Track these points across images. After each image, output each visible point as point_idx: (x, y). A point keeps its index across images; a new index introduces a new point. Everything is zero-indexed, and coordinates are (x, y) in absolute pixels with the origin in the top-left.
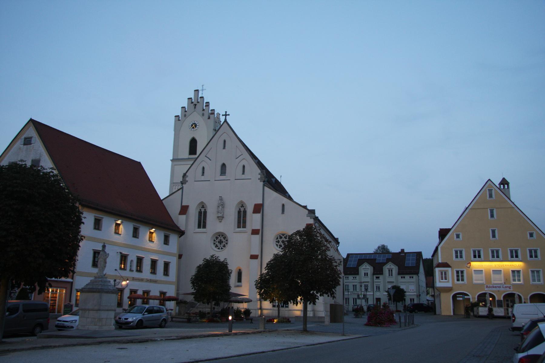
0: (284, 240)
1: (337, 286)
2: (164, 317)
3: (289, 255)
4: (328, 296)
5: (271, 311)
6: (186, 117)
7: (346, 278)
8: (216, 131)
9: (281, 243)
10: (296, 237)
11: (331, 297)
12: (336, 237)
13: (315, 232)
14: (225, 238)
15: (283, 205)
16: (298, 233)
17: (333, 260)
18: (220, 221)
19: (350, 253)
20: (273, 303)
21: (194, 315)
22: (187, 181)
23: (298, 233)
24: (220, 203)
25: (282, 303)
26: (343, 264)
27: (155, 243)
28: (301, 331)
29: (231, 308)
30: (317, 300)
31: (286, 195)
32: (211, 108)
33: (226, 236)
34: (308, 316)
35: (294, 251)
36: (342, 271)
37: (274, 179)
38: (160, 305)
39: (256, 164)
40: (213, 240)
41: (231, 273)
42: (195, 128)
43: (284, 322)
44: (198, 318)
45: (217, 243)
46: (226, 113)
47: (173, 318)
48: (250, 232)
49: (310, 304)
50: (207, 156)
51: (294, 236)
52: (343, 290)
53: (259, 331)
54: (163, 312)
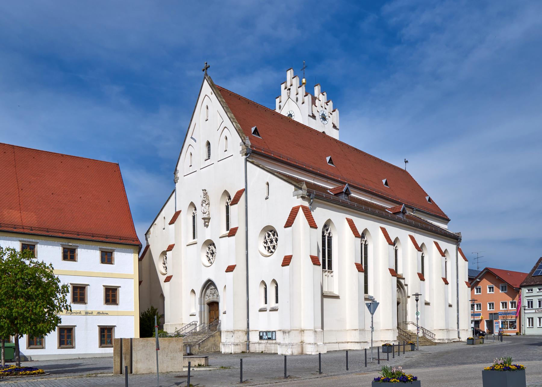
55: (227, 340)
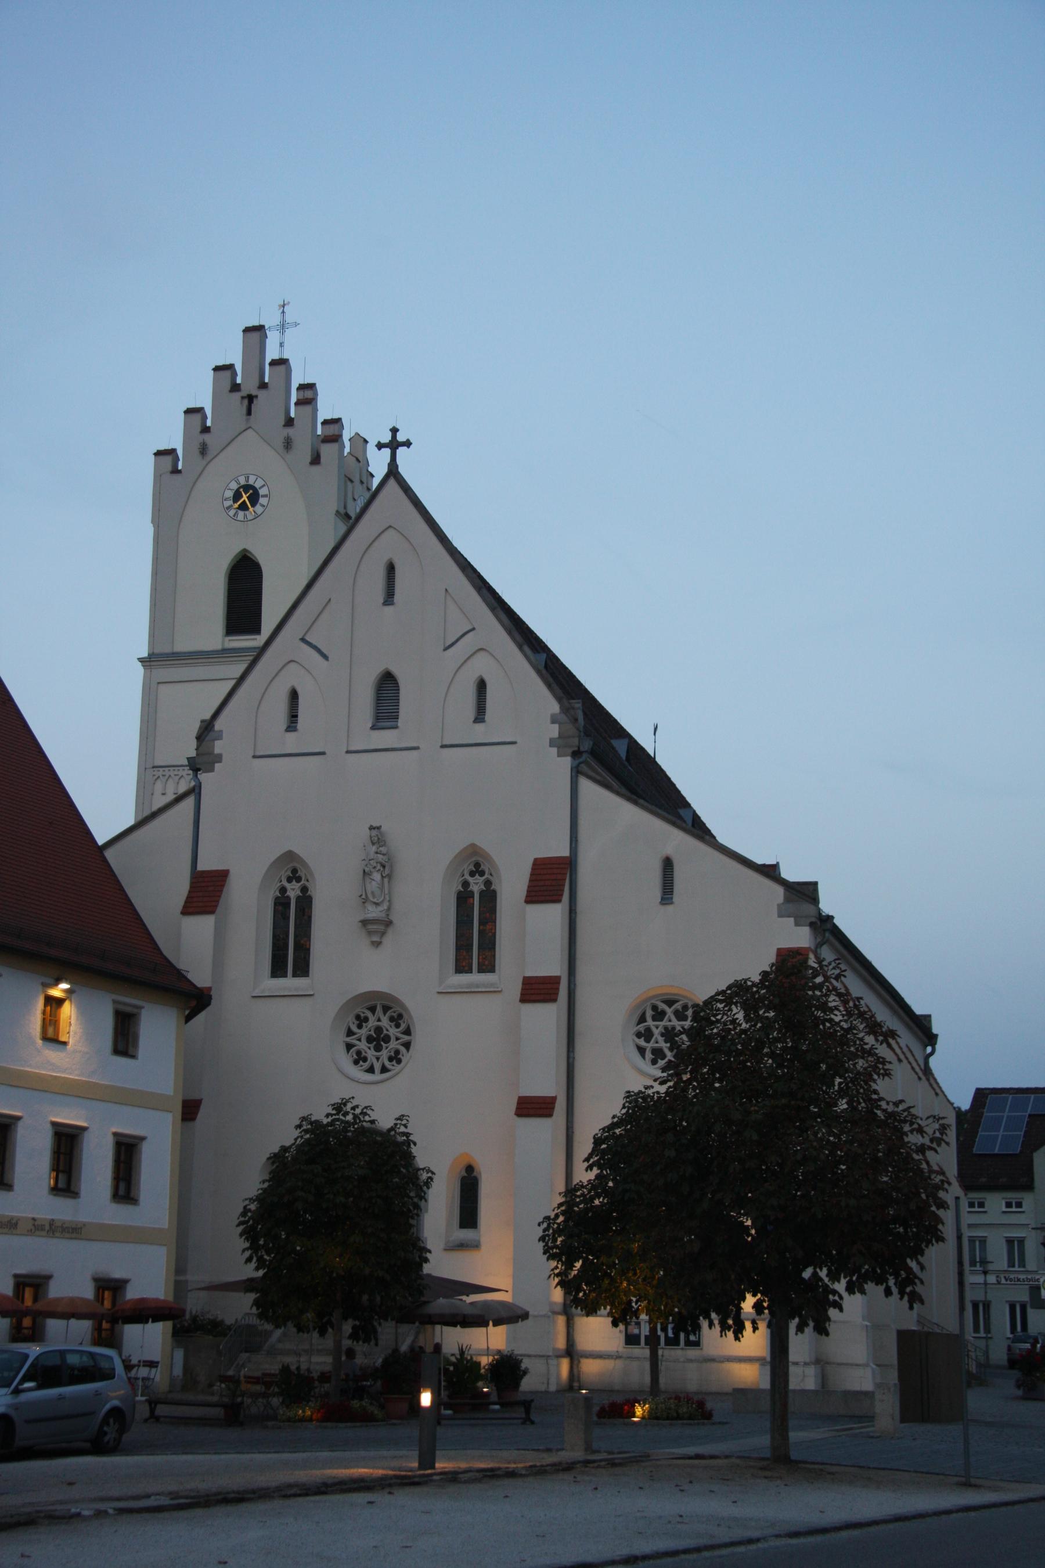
0: (674, 1028)
1: (929, 1243)
2: (116, 1403)
3: (694, 1097)
4: (888, 1292)
5: (619, 1363)
6: (208, 458)
7: (971, 1205)
8: (350, 521)
9: (661, 1039)
10: (730, 1010)
11: (901, 1299)
12: (919, 1010)
13: (819, 987)
14: (396, 1020)
15: (668, 864)
16: (737, 994)
17: (905, 1121)
18: (376, 939)
19: (991, 1086)
20: (627, 1324)
21: (258, 1388)
22: (219, 758)
23: (737, 994)
24: (372, 855)
25: (670, 1326)
26: (958, 1139)
27: (69, 1047)
28: (765, 1463)
29: (429, 1349)
30: (833, 1313)
31: (680, 818)
32: (324, 413)
33: (400, 1010)
34: (792, 1386)
35: (720, 1080)
36: (952, 1170)
37: (626, 741)
38: (98, 1342)
39: (539, 672)
40: (343, 1031)
41: (428, 1183)
42: (251, 509)
43: (678, 1417)
44: (275, 1401)
45: (363, 1045)
46: (394, 436)
47: (159, 1406)
48: (516, 989)
49: (800, 1329)
50: (307, 638)
51: (719, 1010)
52: (960, 1263)
53: (560, 1463)
54: (108, 1375)
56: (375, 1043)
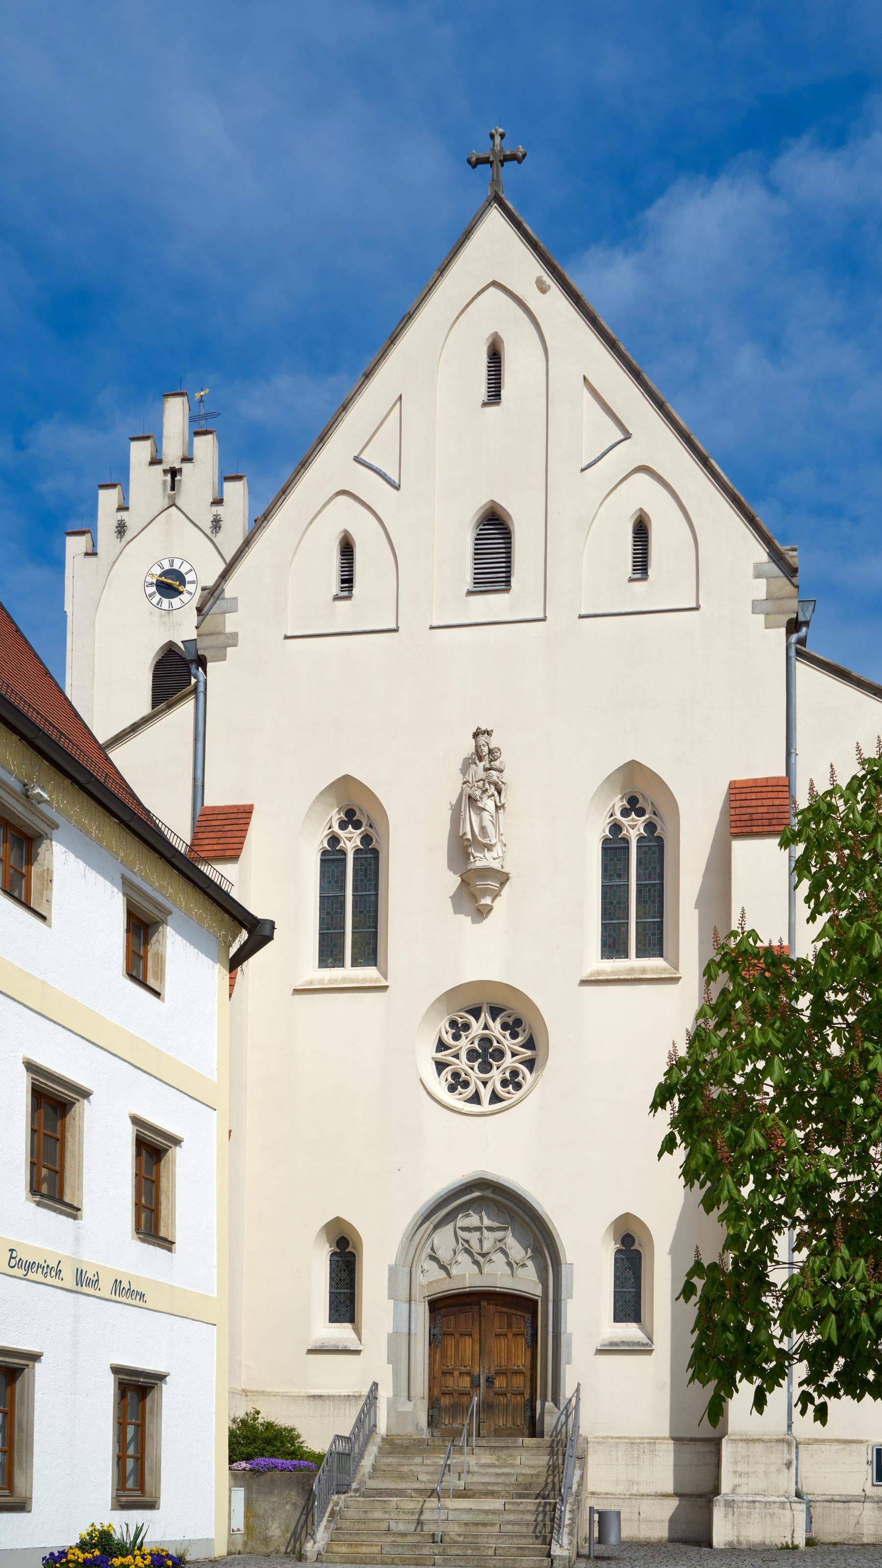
22: (233, 640)
45: (463, 1064)
50: (364, 457)
55: (743, 1480)
56: (480, 1060)
